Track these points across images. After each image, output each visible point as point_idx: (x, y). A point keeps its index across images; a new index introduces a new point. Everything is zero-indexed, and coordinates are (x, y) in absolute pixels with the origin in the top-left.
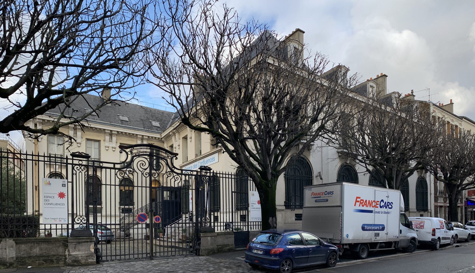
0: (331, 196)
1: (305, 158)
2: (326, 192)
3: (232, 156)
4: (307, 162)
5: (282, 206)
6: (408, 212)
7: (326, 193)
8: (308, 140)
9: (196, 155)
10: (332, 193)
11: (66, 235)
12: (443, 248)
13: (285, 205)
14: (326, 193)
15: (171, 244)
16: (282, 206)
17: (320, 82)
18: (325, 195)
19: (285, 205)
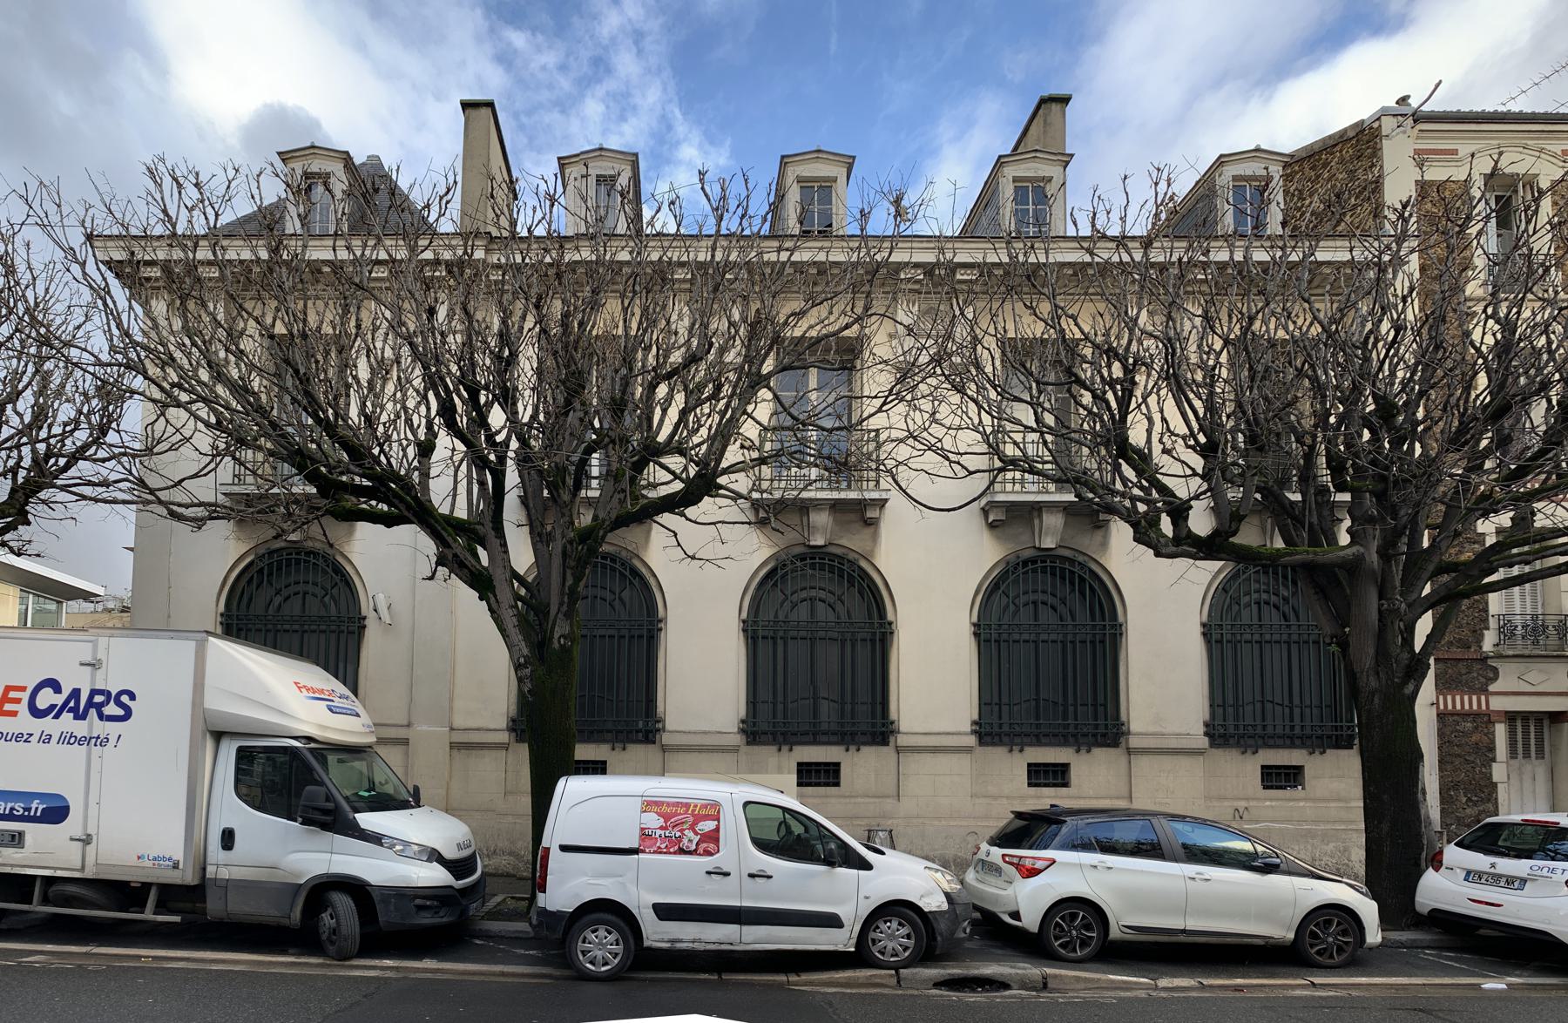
0: (102, 741)
1: (1081, 559)
2: (55, 685)
3: (1155, 483)
4: (1092, 572)
5: (966, 734)
6: (887, 752)
7: (46, 698)
8: (527, 260)
9: (1013, 151)
10: (112, 709)
11: (154, 303)
12: (724, 947)
13: (974, 732)
14: (46, 698)
15: (1199, 316)
16: (966, 734)
17: (1143, 481)
18: (37, 713)
19: (974, 732)
